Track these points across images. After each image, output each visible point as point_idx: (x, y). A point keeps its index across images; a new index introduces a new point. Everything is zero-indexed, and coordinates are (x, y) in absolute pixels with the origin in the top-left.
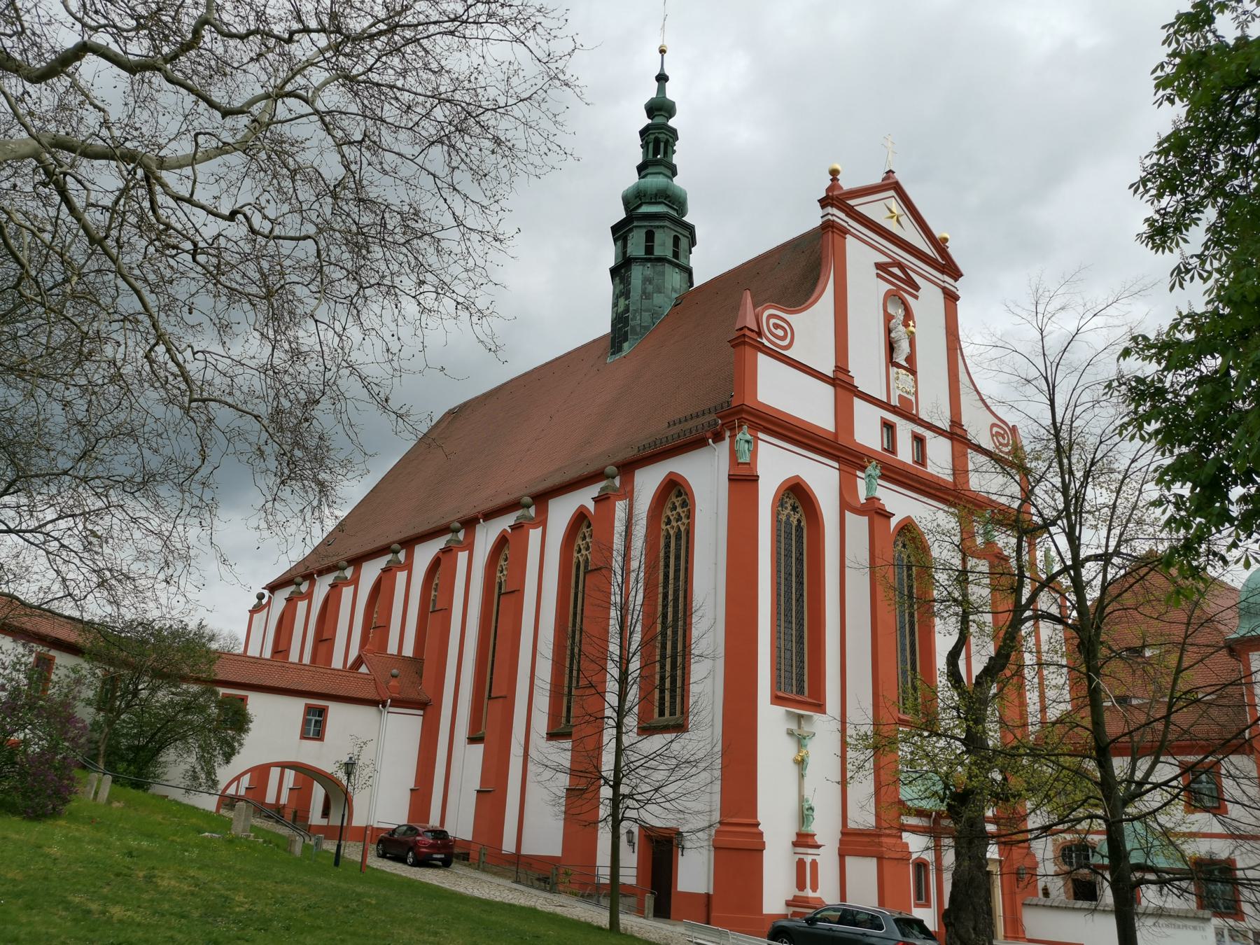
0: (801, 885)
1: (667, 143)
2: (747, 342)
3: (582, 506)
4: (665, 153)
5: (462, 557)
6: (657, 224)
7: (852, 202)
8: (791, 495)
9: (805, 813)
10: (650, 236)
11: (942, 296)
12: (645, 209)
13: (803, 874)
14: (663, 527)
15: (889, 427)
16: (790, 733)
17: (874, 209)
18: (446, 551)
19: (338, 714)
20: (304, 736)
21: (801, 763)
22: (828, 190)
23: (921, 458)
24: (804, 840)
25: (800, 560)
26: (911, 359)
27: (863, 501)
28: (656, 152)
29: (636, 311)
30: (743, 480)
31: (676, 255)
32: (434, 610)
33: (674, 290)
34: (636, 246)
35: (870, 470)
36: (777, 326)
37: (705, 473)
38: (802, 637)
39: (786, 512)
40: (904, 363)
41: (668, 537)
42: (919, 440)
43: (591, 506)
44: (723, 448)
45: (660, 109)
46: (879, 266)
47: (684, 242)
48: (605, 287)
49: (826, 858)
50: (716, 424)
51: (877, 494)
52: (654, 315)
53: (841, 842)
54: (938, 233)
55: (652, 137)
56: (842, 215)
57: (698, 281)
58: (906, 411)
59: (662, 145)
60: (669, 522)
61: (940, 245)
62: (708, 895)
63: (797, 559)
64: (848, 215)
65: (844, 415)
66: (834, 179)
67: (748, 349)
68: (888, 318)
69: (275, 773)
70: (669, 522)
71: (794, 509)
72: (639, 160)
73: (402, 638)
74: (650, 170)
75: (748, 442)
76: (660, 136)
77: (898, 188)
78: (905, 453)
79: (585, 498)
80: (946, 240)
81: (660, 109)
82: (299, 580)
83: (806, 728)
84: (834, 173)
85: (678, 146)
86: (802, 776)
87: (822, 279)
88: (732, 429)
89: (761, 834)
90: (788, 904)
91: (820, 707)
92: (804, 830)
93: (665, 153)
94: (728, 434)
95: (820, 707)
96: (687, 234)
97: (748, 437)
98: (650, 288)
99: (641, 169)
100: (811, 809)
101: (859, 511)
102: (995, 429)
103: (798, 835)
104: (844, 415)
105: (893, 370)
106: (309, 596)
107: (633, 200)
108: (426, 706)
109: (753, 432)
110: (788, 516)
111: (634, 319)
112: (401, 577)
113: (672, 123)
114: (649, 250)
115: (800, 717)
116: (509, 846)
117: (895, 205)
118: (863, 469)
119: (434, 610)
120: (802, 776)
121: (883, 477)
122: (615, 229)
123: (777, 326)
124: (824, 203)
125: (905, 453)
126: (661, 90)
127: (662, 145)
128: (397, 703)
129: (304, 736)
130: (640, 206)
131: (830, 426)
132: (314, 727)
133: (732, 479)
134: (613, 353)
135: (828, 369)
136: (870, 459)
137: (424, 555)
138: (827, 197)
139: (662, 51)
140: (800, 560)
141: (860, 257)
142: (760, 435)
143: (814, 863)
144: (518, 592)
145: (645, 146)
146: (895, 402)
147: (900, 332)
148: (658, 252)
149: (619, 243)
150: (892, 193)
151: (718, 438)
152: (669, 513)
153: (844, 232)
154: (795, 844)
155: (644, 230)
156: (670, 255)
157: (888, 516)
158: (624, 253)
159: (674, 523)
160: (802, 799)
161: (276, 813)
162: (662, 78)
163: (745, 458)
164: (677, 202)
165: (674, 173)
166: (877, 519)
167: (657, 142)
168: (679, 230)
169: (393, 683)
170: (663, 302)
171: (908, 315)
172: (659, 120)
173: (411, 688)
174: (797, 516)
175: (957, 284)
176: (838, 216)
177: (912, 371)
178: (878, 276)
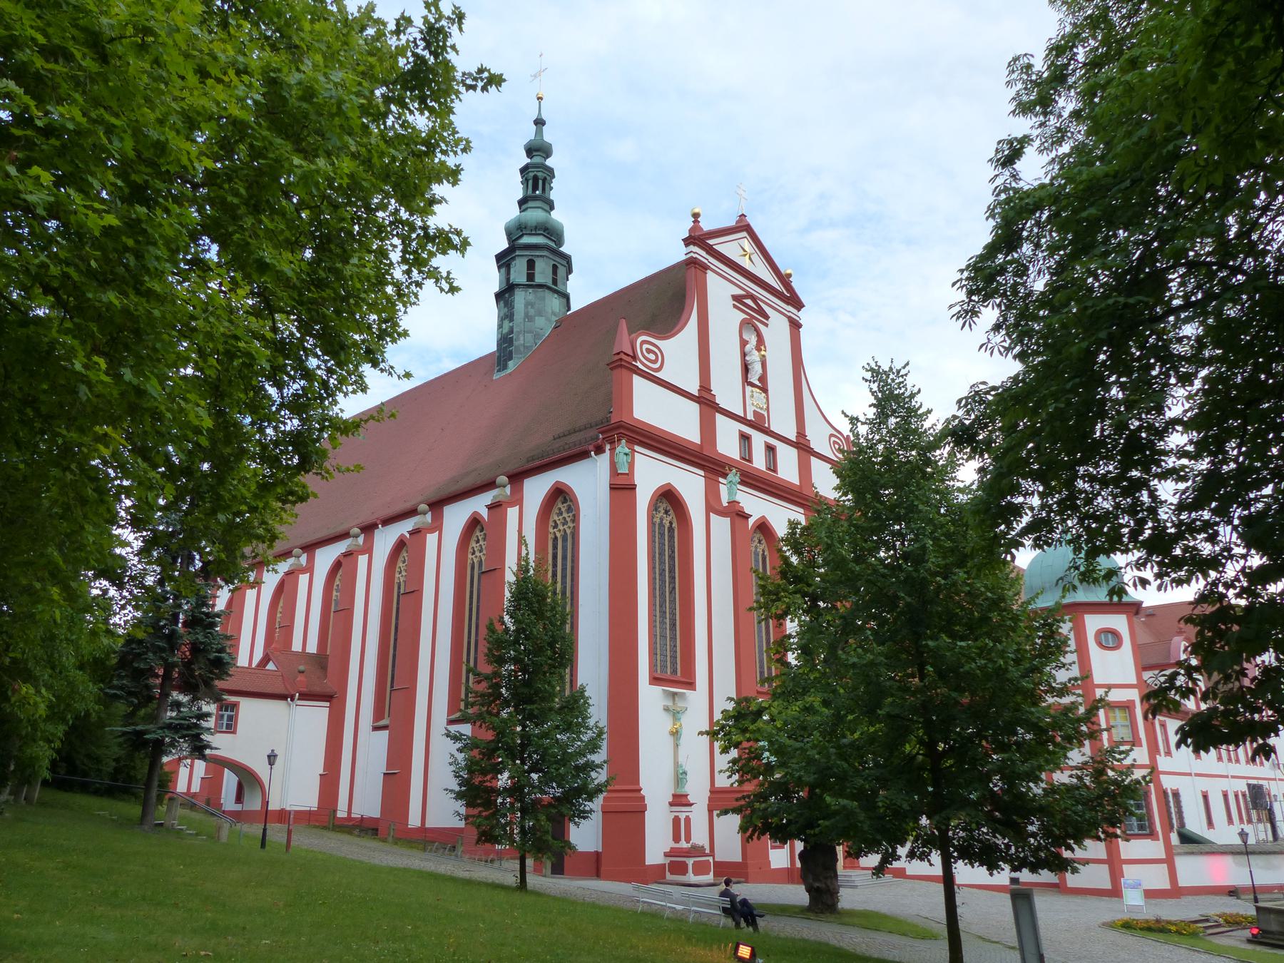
0: (676, 838)
1: (544, 180)
2: (625, 365)
3: (475, 513)
4: (544, 189)
7: (711, 242)
9: (680, 777)
10: (531, 265)
12: (526, 240)
13: (679, 828)
14: (551, 530)
15: (745, 438)
16: (667, 709)
17: (732, 248)
21: (676, 734)
22: (690, 231)
23: (773, 466)
24: (680, 800)
25: (672, 558)
26: (763, 378)
27: (725, 504)
28: (535, 188)
29: (519, 333)
30: (622, 488)
31: (555, 282)
32: (337, 614)
33: (554, 313)
35: (730, 477)
36: (649, 351)
37: (588, 481)
38: (675, 625)
39: (659, 515)
40: (757, 383)
41: (556, 538)
42: (770, 449)
43: (484, 513)
45: (538, 149)
46: (735, 298)
49: (698, 815)
50: (598, 438)
51: (737, 499)
52: (537, 336)
53: (710, 799)
55: (531, 175)
56: (703, 253)
57: (576, 305)
58: (759, 424)
60: (556, 526)
61: (785, 279)
62: (597, 853)
64: (708, 253)
65: (708, 429)
66: (696, 222)
67: (625, 372)
68: (744, 343)
71: (666, 512)
72: (520, 196)
74: (530, 204)
76: (540, 174)
77: (748, 229)
78: (759, 462)
80: (790, 275)
81: (538, 149)
83: (680, 704)
85: (555, 183)
86: (677, 746)
87: (688, 302)
88: (612, 443)
89: (643, 798)
90: (666, 855)
91: (691, 685)
92: (680, 791)
93: (544, 189)
94: (608, 447)
95: (691, 685)
98: (532, 312)
99: (522, 203)
100: (685, 773)
101: (722, 513)
102: (833, 439)
103: (674, 796)
104: (708, 429)
105: (748, 389)
107: (515, 232)
108: (332, 697)
110: (662, 519)
111: (518, 339)
112: (303, 579)
113: (549, 162)
114: (531, 277)
115: (675, 694)
117: (747, 244)
118: (725, 476)
119: (337, 614)
120: (677, 746)
121: (743, 483)
123: (649, 351)
124: (688, 241)
125: (759, 462)
126: (539, 132)
128: (304, 696)
133: (614, 488)
135: (694, 388)
136: (731, 467)
139: (540, 98)
140: (672, 558)
141: (719, 290)
142: (637, 448)
143: (688, 820)
144: (416, 593)
145: (525, 182)
146: (750, 416)
147: (754, 357)
148: (539, 279)
149: (503, 270)
150: (744, 234)
151: (599, 450)
153: (705, 268)
154: (671, 804)
156: (550, 283)
157: (746, 517)
158: (508, 279)
159: (561, 527)
160: (677, 765)
162: (539, 123)
163: (623, 469)
164: (554, 234)
165: (552, 208)
166: (738, 520)
167: (536, 179)
169: (300, 678)
170: (545, 326)
171: (760, 341)
172: (537, 160)
175: (800, 314)
177: (764, 390)
178: (735, 306)
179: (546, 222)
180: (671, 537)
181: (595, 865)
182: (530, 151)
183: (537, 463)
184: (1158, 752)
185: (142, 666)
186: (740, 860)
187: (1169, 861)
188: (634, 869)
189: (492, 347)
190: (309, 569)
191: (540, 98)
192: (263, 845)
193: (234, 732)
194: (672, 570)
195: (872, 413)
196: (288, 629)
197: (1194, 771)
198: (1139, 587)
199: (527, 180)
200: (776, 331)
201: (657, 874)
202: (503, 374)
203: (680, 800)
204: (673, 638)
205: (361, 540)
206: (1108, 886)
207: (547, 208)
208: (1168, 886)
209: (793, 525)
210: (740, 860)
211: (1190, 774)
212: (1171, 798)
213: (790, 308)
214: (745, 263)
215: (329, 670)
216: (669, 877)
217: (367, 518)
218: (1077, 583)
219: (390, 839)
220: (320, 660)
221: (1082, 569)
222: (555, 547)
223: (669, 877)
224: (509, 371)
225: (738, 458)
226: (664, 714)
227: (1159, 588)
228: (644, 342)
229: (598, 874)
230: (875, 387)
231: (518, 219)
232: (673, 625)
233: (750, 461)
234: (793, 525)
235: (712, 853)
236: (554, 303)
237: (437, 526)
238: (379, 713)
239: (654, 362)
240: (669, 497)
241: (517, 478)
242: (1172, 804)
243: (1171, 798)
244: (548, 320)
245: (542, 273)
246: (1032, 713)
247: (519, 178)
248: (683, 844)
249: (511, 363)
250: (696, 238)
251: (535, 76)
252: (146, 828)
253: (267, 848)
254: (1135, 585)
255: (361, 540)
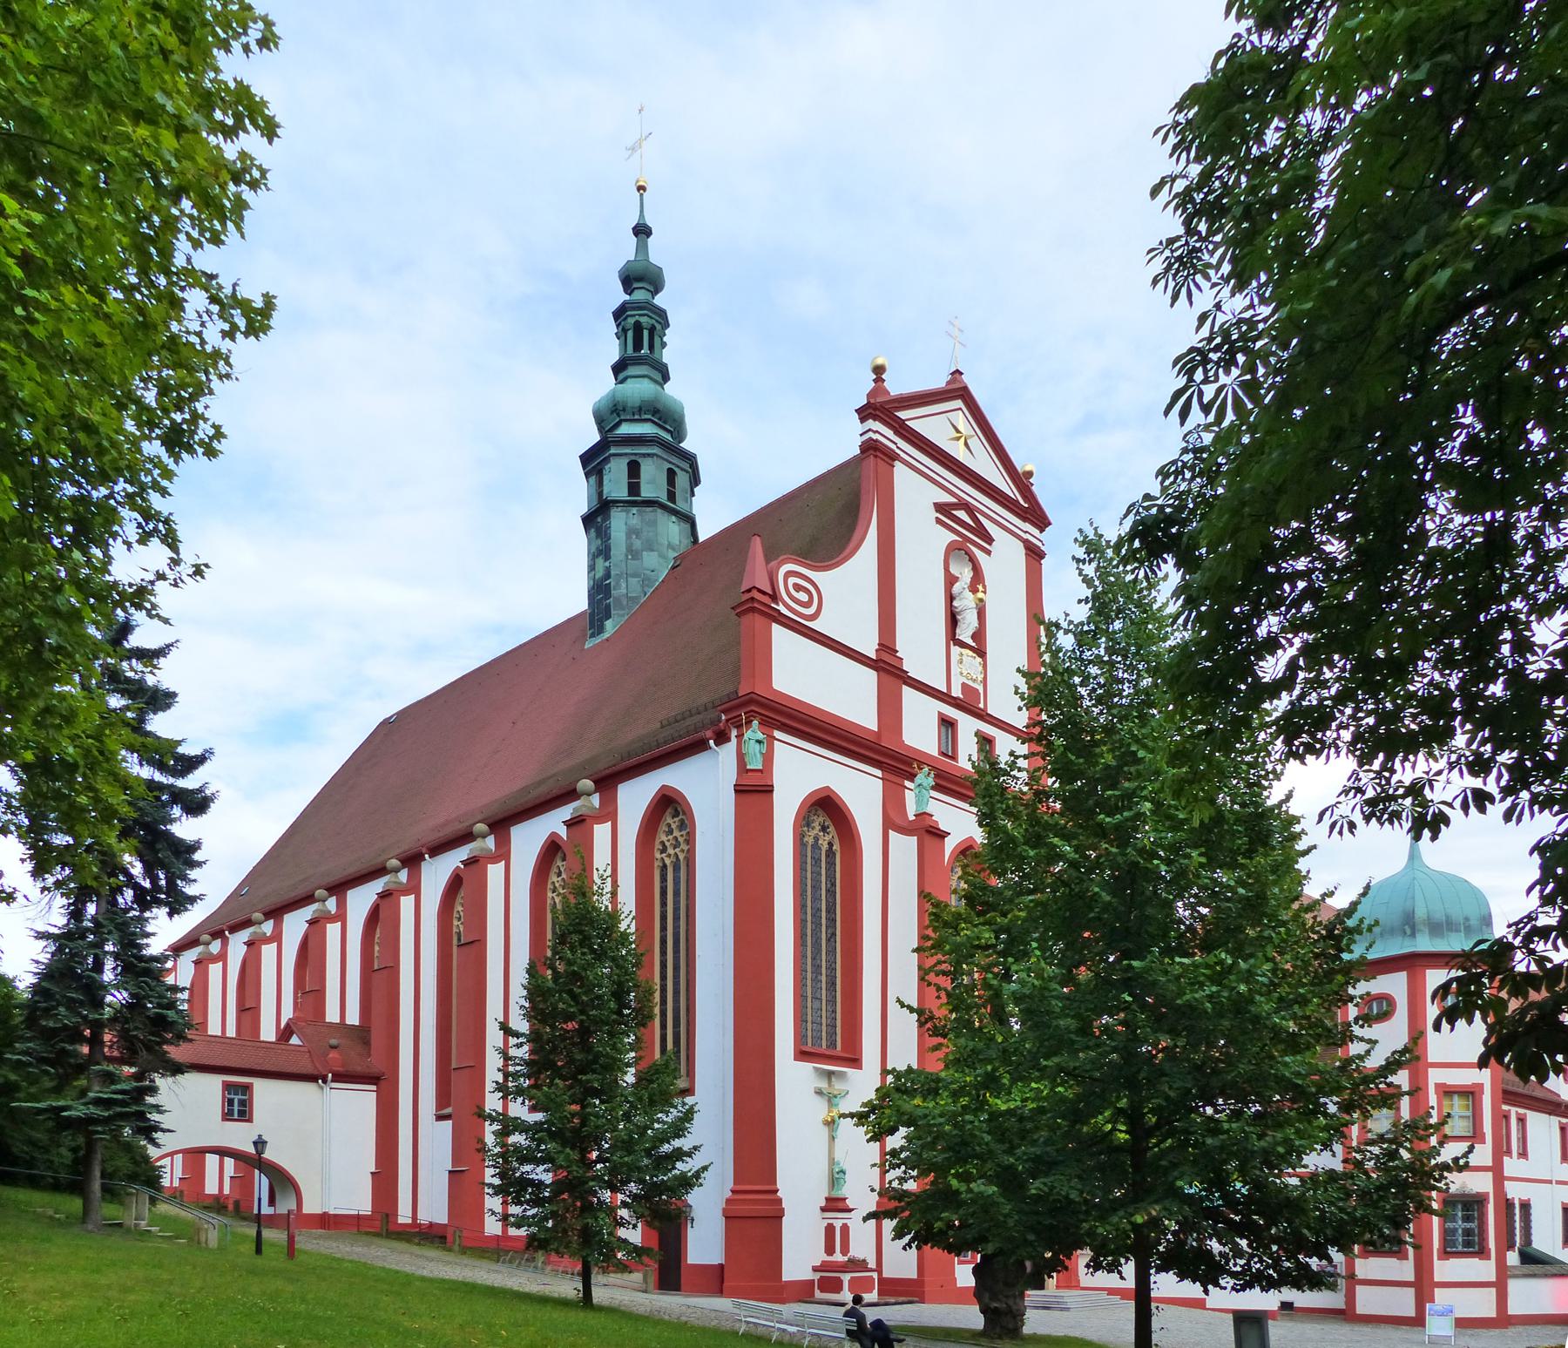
0: (830, 1250)
1: (652, 330)
2: (760, 608)
3: (554, 834)
4: (651, 347)
5: (407, 902)
6: (643, 450)
7: (903, 415)
8: (820, 812)
9: (836, 1176)
10: (634, 469)
11: (1023, 551)
12: (626, 429)
14: (658, 855)
15: (947, 724)
16: (819, 1092)
17: (935, 425)
18: (385, 895)
19: (265, 1093)
20: (227, 1116)
24: (835, 1204)
25: (831, 892)
26: (979, 635)
27: (912, 818)
28: (638, 345)
29: (619, 576)
30: (754, 791)
31: (672, 496)
32: (379, 976)
33: (670, 546)
34: (616, 486)
35: (920, 778)
36: (798, 588)
37: (707, 782)
38: (834, 984)
41: (664, 867)
43: (563, 832)
44: (728, 752)
45: (641, 278)
46: (940, 507)
47: (682, 480)
48: (578, 542)
52: (646, 581)
54: (1021, 465)
55: (631, 321)
56: (889, 433)
57: (703, 536)
58: (970, 704)
59: (646, 333)
60: (664, 850)
61: (1022, 480)
62: (721, 1266)
63: (827, 891)
64: (897, 433)
65: (890, 708)
66: (879, 380)
67: (758, 620)
68: (951, 580)
69: (212, 1161)
70: (664, 850)
71: (824, 829)
72: (615, 357)
73: (343, 1003)
74: (631, 371)
75: (759, 742)
76: (643, 320)
77: (964, 394)
79: (554, 822)
80: (1030, 474)
81: (641, 278)
82: (206, 937)
83: (838, 1086)
84: (879, 370)
85: (670, 336)
87: (862, 514)
88: (739, 727)
89: (780, 1201)
90: (815, 1269)
91: (855, 1062)
93: (651, 347)
94: (734, 733)
95: (855, 1062)
96: (687, 466)
97: (760, 736)
98: (637, 544)
99: (619, 368)
101: (905, 830)
103: (827, 1199)
104: (890, 708)
105: (955, 650)
106: (222, 957)
107: (610, 415)
108: (382, 1080)
109: (767, 730)
110: (816, 839)
111: (618, 586)
112: (333, 930)
114: (634, 488)
115: (830, 1074)
116: (404, 1216)
117: (963, 421)
118: (912, 777)
119: (379, 976)
122: (586, 459)
123: (798, 588)
124: (865, 413)
126: (642, 248)
127: (646, 333)
128: (340, 1077)
129: (227, 1116)
130: (618, 425)
131: (873, 725)
132: (238, 1108)
133: (740, 790)
134: (592, 636)
135: (870, 649)
136: (921, 764)
137: (361, 901)
138: (868, 406)
139: (641, 188)
140: (831, 892)
141: (914, 494)
142: (777, 734)
143: (845, 1229)
145: (622, 334)
146: (957, 692)
147: (966, 602)
148: (647, 492)
149: (593, 479)
150: (959, 403)
151: (722, 738)
152: (664, 838)
153: (891, 457)
154: (823, 1210)
155: (625, 461)
156: (664, 499)
157: (941, 835)
158: (600, 494)
159: (671, 851)
161: (218, 1205)
163: (755, 763)
164: (669, 420)
165: (666, 378)
166: (928, 839)
167: (638, 328)
168: (675, 460)
169: (333, 1054)
170: (658, 565)
171: (978, 577)
173: (360, 1058)
174: (827, 838)
176: (883, 432)
177: (981, 652)
178: (938, 521)
179: (656, 399)
180: (831, 864)
181: (715, 1280)
182: (629, 280)
183: (633, 761)
184: (1509, 1153)
185: (51, 1024)
186: (915, 1276)
187: (1500, 1286)
188: (776, 1289)
189: (581, 604)
190: (341, 916)
191: (641, 188)
192: (259, 1251)
193: (250, 1120)
194: (831, 910)
195: (1081, 613)
196: (319, 994)
197: (1555, 1179)
198: (1473, 810)
199: (625, 331)
200: (1004, 561)
201: (803, 1292)
202: (598, 640)
203: (835, 1204)
204: (832, 1001)
205: (403, 876)
206: (1412, 1313)
207: (658, 377)
208: (1493, 1314)
209: (71, 84)
210: (915, 1276)
211: (1550, 1182)
212: (1517, 1211)
213: (1027, 527)
214: (958, 452)
215: (373, 1043)
216: (818, 1294)
217: (407, 845)
218: (1357, 817)
219: (456, 1248)
220: (361, 1034)
221: (1370, 793)
222: (664, 879)
223: (818, 1294)
224: (606, 635)
225: (935, 753)
226: (817, 1098)
227: (1508, 816)
228: (789, 574)
229: (720, 1292)
230: (1090, 570)
231: (614, 391)
232: (832, 984)
233: (954, 757)
234: (71, 84)
235: (879, 1269)
236: (672, 530)
237: (503, 853)
238: (443, 1097)
239: (807, 605)
240: (826, 808)
241: (608, 782)
242: (1517, 1218)
243: (1517, 1211)
244: (662, 556)
245: (652, 482)
246: (1286, 1064)
247: (612, 327)
248: (838, 1257)
249: (609, 624)
250: (879, 408)
251: (633, 149)
252: (90, 1227)
253: (300, 1258)
254: (1465, 807)
255: (403, 876)
